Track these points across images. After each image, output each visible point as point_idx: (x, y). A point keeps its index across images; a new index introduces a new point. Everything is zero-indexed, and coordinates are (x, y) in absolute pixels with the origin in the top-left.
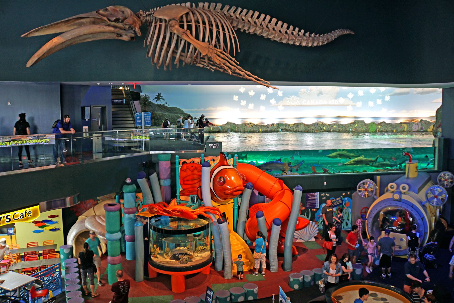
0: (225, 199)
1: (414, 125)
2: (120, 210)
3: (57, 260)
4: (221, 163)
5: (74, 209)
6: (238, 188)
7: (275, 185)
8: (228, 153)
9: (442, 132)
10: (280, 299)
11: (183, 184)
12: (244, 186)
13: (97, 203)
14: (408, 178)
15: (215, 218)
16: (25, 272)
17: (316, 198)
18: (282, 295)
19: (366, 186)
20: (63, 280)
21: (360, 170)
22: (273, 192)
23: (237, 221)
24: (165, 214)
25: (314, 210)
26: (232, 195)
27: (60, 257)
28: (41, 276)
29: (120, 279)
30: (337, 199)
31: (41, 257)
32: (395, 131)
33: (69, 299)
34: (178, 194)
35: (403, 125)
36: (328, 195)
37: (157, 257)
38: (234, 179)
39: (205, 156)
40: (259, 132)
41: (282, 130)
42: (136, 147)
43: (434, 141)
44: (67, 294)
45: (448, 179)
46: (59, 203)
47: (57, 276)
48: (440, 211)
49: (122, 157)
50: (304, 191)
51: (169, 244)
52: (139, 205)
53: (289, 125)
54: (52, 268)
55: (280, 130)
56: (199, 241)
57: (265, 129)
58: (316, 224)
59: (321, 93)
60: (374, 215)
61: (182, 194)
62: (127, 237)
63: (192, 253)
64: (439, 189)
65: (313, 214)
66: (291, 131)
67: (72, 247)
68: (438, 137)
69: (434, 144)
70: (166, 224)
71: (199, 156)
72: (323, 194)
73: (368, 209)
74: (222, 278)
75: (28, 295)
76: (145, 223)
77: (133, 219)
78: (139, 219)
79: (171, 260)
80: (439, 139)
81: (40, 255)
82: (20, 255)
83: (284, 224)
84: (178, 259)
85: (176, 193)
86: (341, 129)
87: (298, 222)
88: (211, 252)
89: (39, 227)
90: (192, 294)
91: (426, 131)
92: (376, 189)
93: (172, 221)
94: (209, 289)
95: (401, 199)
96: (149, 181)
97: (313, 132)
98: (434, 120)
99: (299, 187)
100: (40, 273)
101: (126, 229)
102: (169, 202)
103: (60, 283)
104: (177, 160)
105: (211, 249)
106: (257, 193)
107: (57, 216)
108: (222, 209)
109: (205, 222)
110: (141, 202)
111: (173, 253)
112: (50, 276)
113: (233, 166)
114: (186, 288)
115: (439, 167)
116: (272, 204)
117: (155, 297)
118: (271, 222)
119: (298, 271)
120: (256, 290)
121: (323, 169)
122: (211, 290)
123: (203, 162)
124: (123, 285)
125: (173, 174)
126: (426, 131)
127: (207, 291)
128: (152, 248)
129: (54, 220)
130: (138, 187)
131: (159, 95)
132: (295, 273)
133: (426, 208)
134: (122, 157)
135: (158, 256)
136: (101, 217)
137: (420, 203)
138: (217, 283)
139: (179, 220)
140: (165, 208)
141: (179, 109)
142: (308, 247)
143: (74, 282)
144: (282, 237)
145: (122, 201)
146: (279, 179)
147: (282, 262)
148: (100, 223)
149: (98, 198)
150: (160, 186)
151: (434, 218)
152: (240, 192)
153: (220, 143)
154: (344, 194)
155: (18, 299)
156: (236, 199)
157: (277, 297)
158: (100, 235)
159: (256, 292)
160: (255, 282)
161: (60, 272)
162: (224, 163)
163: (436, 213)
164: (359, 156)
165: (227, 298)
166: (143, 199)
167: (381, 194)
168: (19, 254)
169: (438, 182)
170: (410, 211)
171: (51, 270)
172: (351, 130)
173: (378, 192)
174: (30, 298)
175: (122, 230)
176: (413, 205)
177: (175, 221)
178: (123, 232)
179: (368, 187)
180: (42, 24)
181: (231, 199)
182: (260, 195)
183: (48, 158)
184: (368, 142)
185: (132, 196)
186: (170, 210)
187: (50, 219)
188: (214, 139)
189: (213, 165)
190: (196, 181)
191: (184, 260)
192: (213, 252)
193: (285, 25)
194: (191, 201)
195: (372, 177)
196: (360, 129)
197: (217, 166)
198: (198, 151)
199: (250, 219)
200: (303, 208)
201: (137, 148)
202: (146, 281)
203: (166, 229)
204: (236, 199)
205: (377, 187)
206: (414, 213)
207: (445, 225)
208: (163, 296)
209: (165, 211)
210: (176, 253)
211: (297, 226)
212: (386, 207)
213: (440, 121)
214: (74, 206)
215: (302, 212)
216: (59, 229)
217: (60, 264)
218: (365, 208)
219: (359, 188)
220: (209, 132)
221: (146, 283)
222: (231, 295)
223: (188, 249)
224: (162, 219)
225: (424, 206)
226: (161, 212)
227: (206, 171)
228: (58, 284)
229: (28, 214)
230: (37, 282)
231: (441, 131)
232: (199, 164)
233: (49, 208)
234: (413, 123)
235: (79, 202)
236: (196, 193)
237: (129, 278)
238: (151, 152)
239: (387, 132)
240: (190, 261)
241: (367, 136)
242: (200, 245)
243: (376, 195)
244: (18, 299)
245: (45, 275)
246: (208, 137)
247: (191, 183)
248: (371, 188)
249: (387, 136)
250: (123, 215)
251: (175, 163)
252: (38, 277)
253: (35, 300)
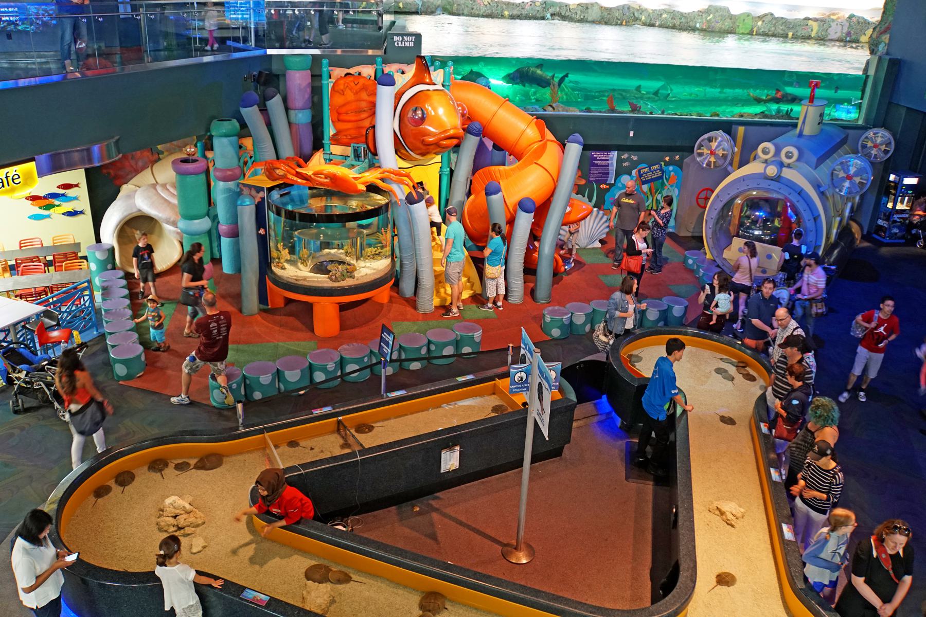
0: (423, 154)
1: (833, 25)
2: (207, 172)
3: (83, 273)
4: (418, 80)
5: (112, 172)
6: (452, 132)
7: (528, 130)
8: (434, 58)
9: (889, 45)
10: (522, 352)
11: (338, 119)
12: (464, 129)
13: (159, 159)
14: (800, 135)
15: (401, 192)
16: (21, 297)
17: (610, 162)
18: (526, 345)
19: (714, 145)
20: (98, 312)
21: (707, 114)
22: (523, 143)
23: (447, 201)
24: (299, 180)
25: (603, 186)
26: (436, 147)
27: (88, 267)
28: (54, 303)
29: (211, 311)
30: (653, 168)
31: (52, 268)
32: (790, 34)
33: (113, 347)
34: (326, 141)
35: (810, 22)
36: (635, 158)
37: (283, 268)
38: (443, 116)
39: (385, 62)
40: (503, 17)
41: (552, 15)
42: (236, 39)
43: (868, 63)
44: (108, 337)
45: (881, 144)
46: (76, 156)
47: (87, 304)
48: (852, 207)
49: (207, 59)
50: (586, 148)
51: (309, 243)
52: (246, 163)
54: (75, 288)
55: (548, 16)
56: (369, 238)
57: (515, 12)
58: (604, 215)
60: (721, 205)
61: (336, 140)
62: (223, 227)
63: (353, 262)
64: (855, 163)
65: (602, 194)
66: (571, 20)
67: (113, 249)
68: (879, 53)
69: (866, 70)
70: (302, 202)
71: (371, 61)
72: (625, 156)
73: (713, 192)
74: (413, 310)
75: (33, 340)
76: (258, 200)
77: (234, 192)
78: (246, 191)
79: (312, 274)
80: (880, 59)
81: (48, 264)
82: (6, 263)
83: (541, 210)
84: (327, 272)
85: (323, 139)
86: (677, 22)
87: (568, 209)
88: (393, 260)
89: (40, 208)
90: (353, 339)
91: (857, 41)
92: (733, 153)
93: (313, 196)
94: (385, 329)
95: (779, 176)
96: (264, 110)
97: (618, 23)
98: (877, 18)
99: (578, 136)
100: (52, 298)
101: (221, 210)
102: (307, 159)
103: (94, 317)
104: (325, 70)
105: (393, 255)
106: (489, 144)
107: (77, 186)
108: (418, 174)
109: (380, 199)
110: (251, 157)
111: (316, 261)
112: (73, 304)
113: (443, 86)
114: (343, 327)
115: (866, 120)
116: (520, 168)
117: (281, 344)
118: (515, 206)
119: (562, 304)
120: (478, 335)
121: (630, 104)
122: (390, 332)
123: (379, 74)
124: (217, 321)
125: (316, 99)
126: (857, 41)
127: (382, 333)
128: (273, 250)
129: (70, 193)
130: (243, 125)
132: (556, 308)
133: (827, 198)
134: (207, 59)
135: (286, 265)
136: (168, 187)
137: (817, 186)
138: (403, 320)
139: (329, 194)
140: (299, 170)
142: (587, 259)
143: (124, 315)
144: (535, 236)
145: (209, 154)
146: (537, 118)
147: (532, 285)
148: (166, 200)
149: (159, 147)
150: (290, 123)
151: (838, 219)
152: (455, 141)
153: (418, 37)
154: (667, 159)
155: (15, 346)
156: (446, 155)
157: (517, 349)
158: (168, 222)
159: (478, 340)
160: (477, 321)
161: (92, 297)
162: (424, 78)
163: (843, 211)
164: (747, 305)
165: (420, 348)
166: (254, 150)
167: (742, 163)
168: (6, 261)
169: (860, 148)
170: (794, 201)
171: (72, 293)
172: (698, 25)
173: (737, 159)
174: (37, 345)
175: (212, 213)
176: (802, 190)
177: (321, 196)
178: (215, 219)
179: (717, 147)
181: (437, 154)
182: (493, 149)
183: (43, 60)
184: (731, 54)
185: (231, 144)
186: (310, 173)
187: (61, 191)
188: (404, 27)
189: (401, 81)
190: (364, 115)
191: (338, 274)
192: (397, 260)
194: (352, 156)
195: (728, 127)
196: (718, 26)
197: (410, 85)
198: (370, 52)
199: (472, 197)
200: (583, 182)
201: (238, 42)
202: (264, 314)
203: (302, 211)
204: (446, 155)
205: (736, 149)
206: (801, 206)
207: (858, 236)
208: (297, 343)
209: (298, 175)
210: (322, 259)
211: (566, 215)
212: (748, 190)
213: (891, 19)
214: (110, 163)
215: (579, 189)
216: (81, 212)
217: (89, 282)
218: (707, 189)
219: (699, 148)
220: (396, 13)
221: (263, 318)
222: (429, 342)
223: (347, 253)
224: (294, 192)
225: (822, 195)
226: (290, 177)
227: (385, 95)
228: (90, 319)
229: (13, 180)
230: (47, 314)
231: (887, 41)
232: (373, 78)
233: (55, 166)
234: (833, 20)
235: (121, 155)
236: (364, 139)
237: (230, 308)
238: (270, 52)
239: (774, 35)
240: (351, 277)
241: (730, 41)
242: (370, 245)
243: (731, 164)
244: (15, 346)
245: (63, 301)
246: (393, 23)
247: (353, 118)
248: (724, 150)
249: (774, 45)
250: (212, 184)
251: (321, 76)
252: (49, 305)
253: (48, 349)
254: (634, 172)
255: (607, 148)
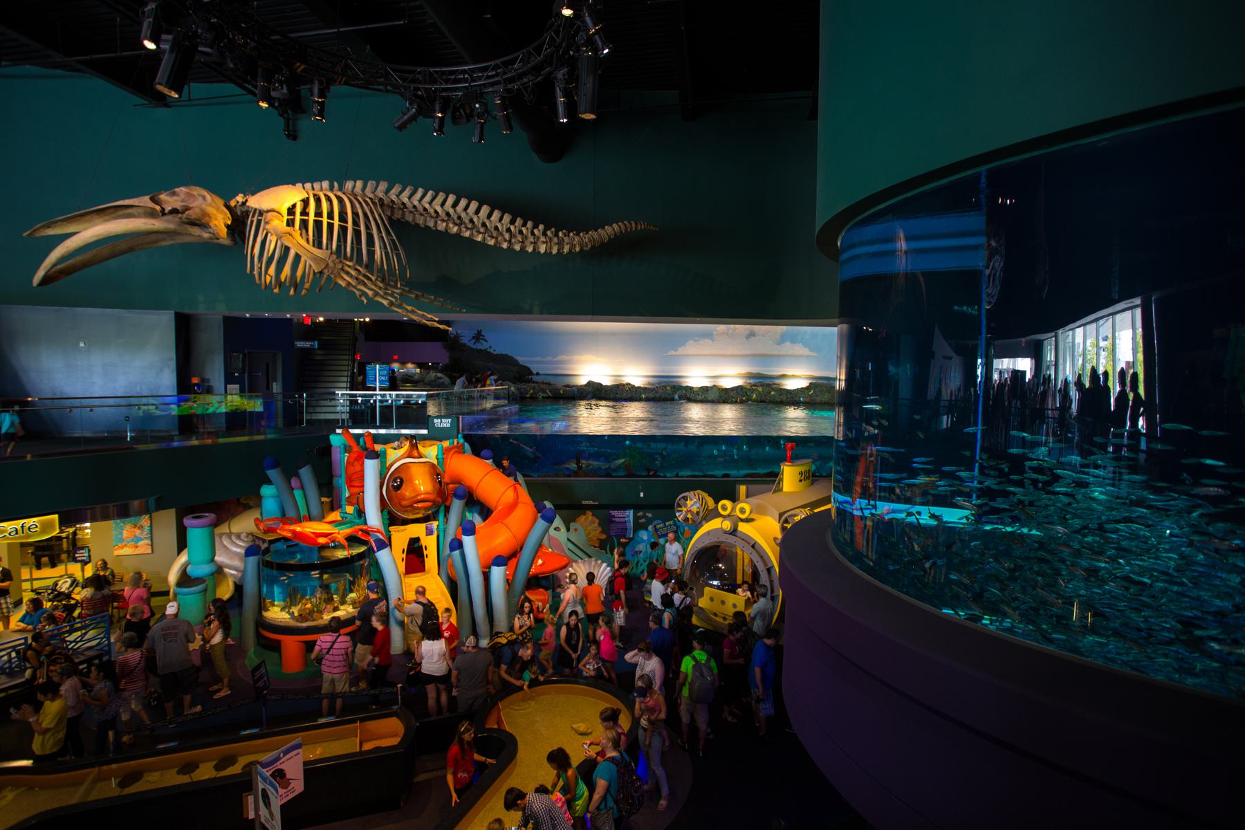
25: (623, 540)
34: (344, 502)
36: (650, 515)
53: (691, 388)
57: (651, 395)
59: (752, 334)
72: (640, 514)
131: (479, 333)
141: (511, 358)
180: (68, 220)
193: (507, 218)
196: (818, 399)
200: (604, 537)
254: (650, 528)
255: (624, 507)
